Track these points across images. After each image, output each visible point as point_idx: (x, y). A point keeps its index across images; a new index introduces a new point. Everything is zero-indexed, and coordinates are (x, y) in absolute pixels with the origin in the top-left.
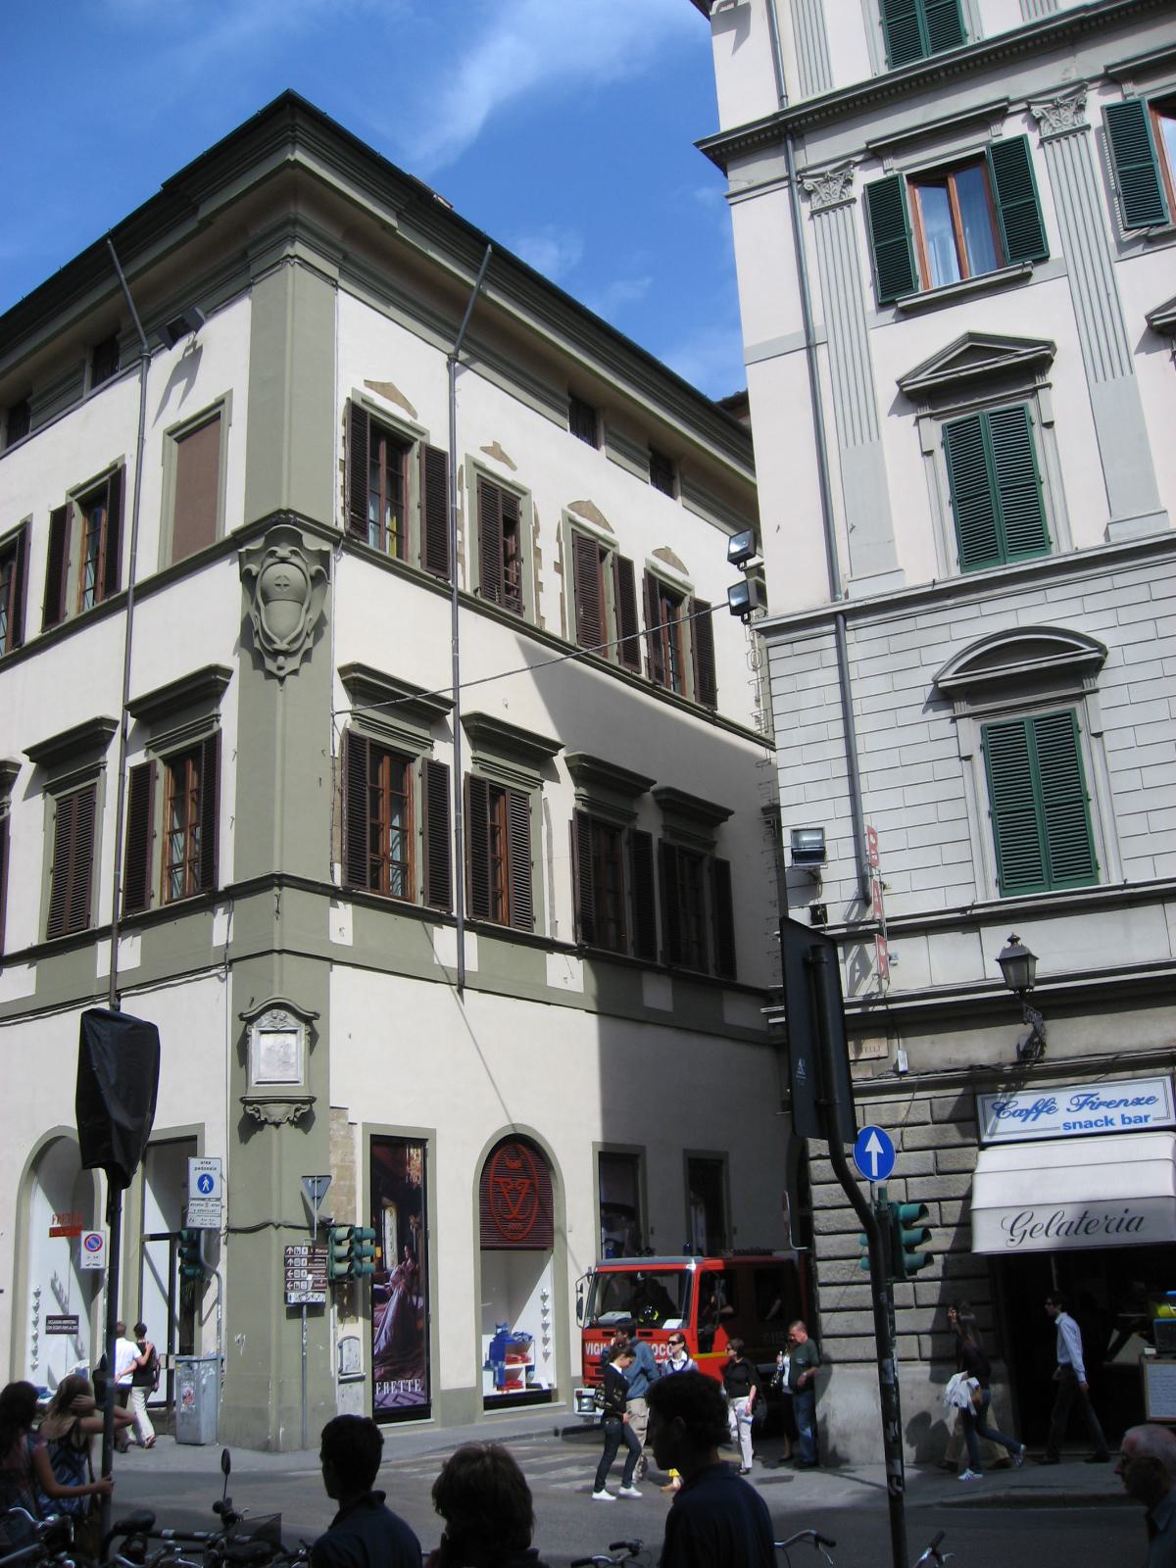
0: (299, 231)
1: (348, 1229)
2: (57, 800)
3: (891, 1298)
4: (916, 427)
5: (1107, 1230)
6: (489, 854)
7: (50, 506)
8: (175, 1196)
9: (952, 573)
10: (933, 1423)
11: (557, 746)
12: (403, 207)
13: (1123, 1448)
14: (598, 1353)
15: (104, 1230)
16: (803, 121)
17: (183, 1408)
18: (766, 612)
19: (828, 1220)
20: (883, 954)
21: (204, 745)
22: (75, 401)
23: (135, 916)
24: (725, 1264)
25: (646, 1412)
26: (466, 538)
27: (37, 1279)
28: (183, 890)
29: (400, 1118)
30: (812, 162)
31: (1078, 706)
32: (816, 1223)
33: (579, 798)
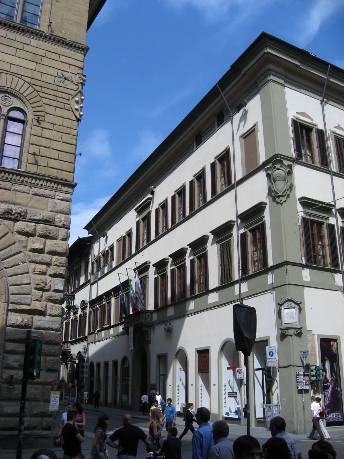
0: (271, 72)
1: (315, 366)
2: (220, 245)
7: (210, 162)
12: (301, 59)
21: (260, 225)
22: (214, 132)
27: (224, 382)
28: (258, 268)
29: (329, 332)
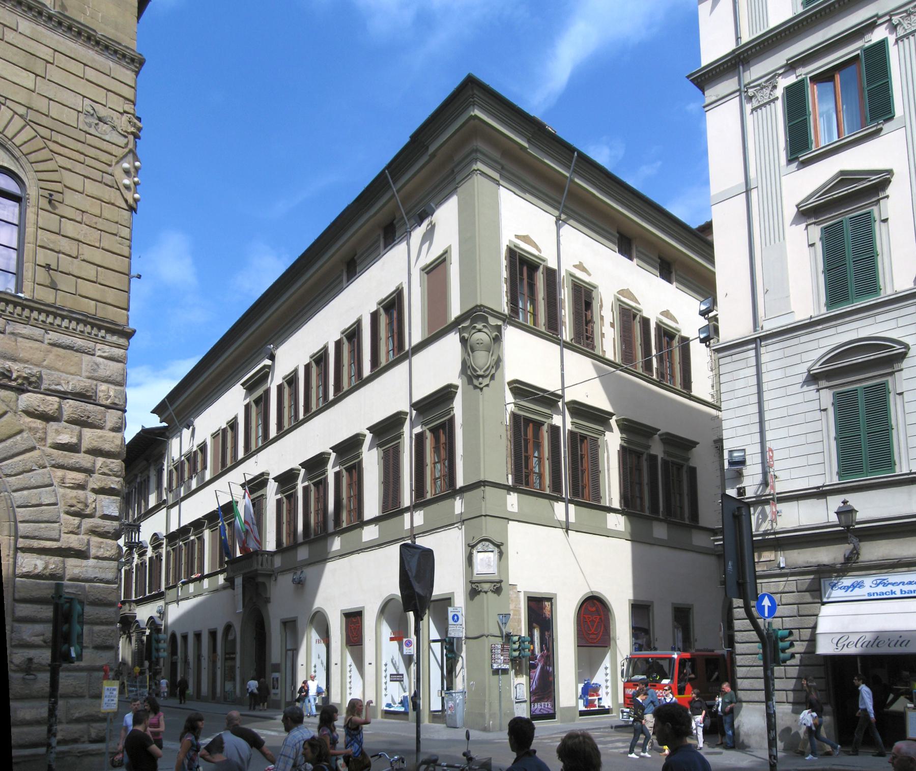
3: (773, 673)
4: (806, 231)
5: (889, 646)
6: (580, 468)
8: (442, 624)
9: (823, 311)
10: (792, 732)
11: (612, 415)
12: (530, 136)
13: (893, 751)
14: (631, 693)
15: (413, 638)
16: (749, 52)
17: (449, 712)
18: (718, 340)
19: (742, 636)
20: (774, 510)
23: (420, 502)
24: (691, 656)
25: (653, 720)
26: (566, 313)
27: (386, 659)
28: (441, 489)
29: (540, 588)
30: (753, 78)
31: (890, 379)
32: (736, 638)
33: (622, 439)
